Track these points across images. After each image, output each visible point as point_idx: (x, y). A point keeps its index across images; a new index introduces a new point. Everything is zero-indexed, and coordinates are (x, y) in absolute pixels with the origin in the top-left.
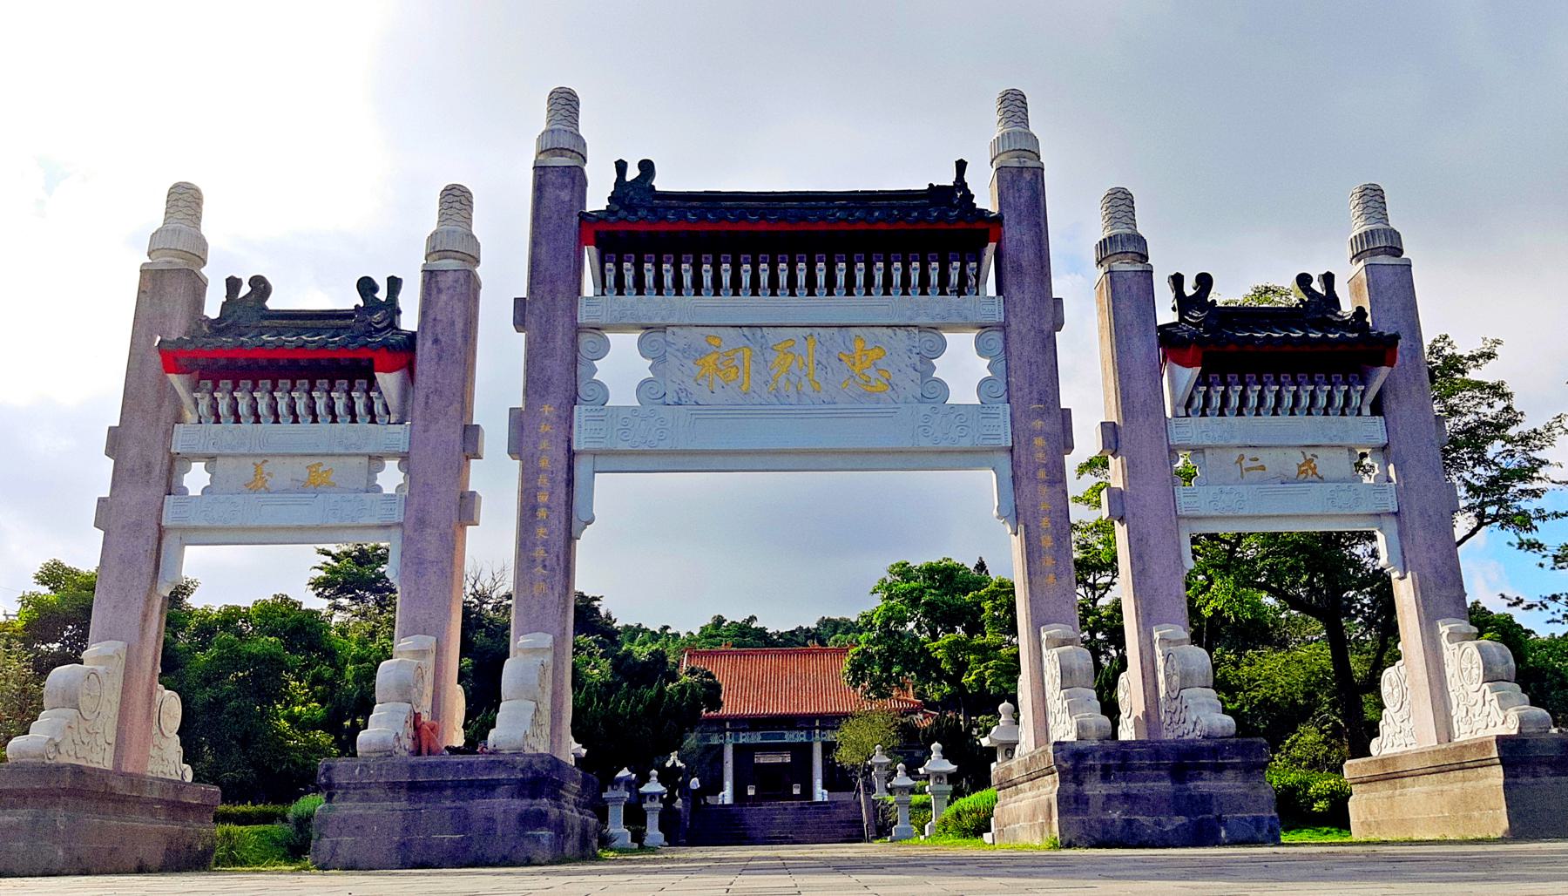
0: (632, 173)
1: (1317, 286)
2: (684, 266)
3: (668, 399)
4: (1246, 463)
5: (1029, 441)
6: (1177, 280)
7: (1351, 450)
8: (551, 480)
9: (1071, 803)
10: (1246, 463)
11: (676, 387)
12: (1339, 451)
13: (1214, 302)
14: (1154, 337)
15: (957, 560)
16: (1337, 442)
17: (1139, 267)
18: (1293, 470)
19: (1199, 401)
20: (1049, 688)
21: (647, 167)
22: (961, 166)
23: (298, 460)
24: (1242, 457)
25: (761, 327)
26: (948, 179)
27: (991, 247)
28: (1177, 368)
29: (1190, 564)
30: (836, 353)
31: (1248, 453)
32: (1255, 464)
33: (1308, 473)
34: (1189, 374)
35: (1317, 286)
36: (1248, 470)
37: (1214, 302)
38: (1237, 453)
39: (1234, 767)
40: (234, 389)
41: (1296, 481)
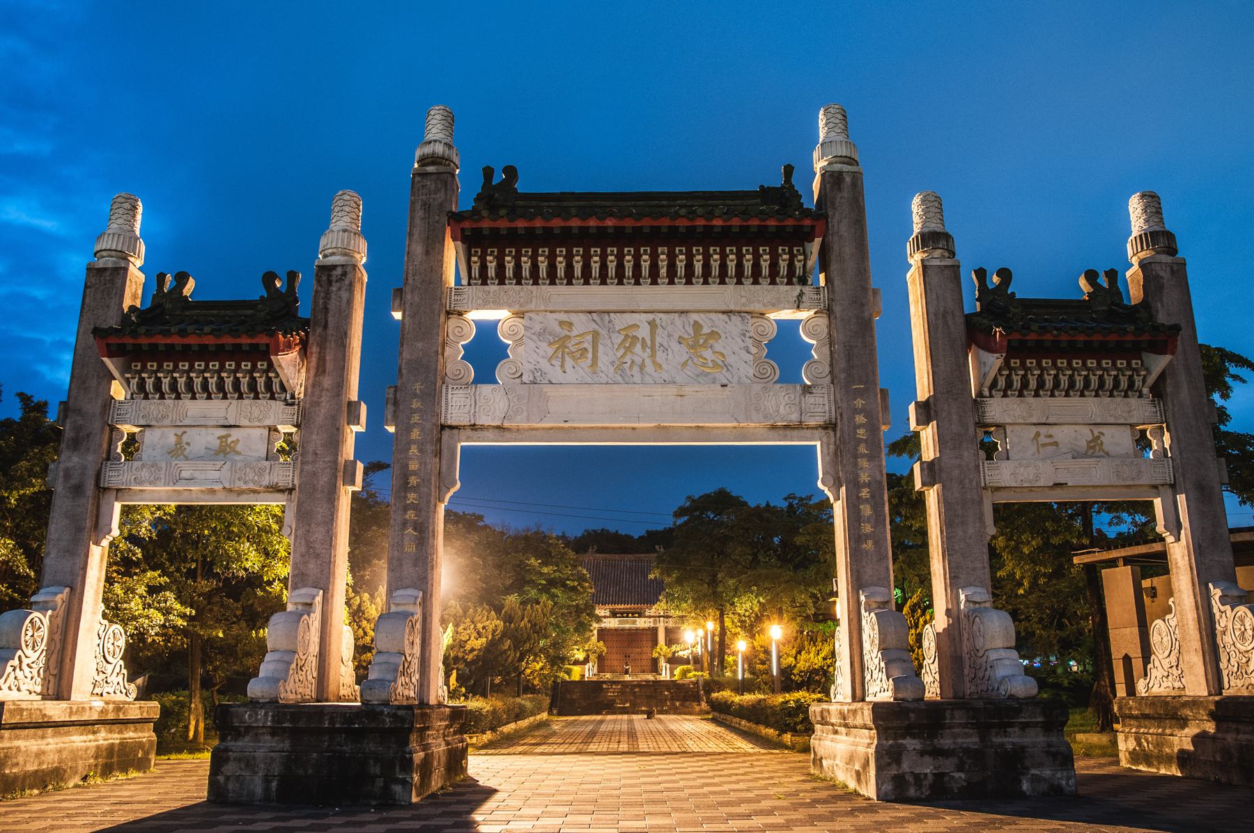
0: (499, 177)
1: (1103, 282)
2: (540, 259)
3: (525, 378)
4: (1042, 440)
5: (851, 419)
6: (981, 274)
7: (1132, 426)
8: (421, 451)
9: (887, 757)
10: (1042, 440)
11: (532, 367)
12: (1122, 428)
13: (1013, 294)
14: (960, 321)
15: (745, 499)
16: (1122, 421)
17: (948, 262)
18: (1083, 444)
19: (1002, 382)
20: (867, 646)
21: (511, 172)
22: (789, 170)
23: (211, 430)
24: (1038, 434)
25: (608, 312)
26: (779, 182)
27: (818, 241)
28: (982, 352)
29: (992, 531)
30: (676, 337)
31: (1043, 430)
32: (1048, 440)
33: (1094, 449)
34: (994, 361)
35: (1103, 282)
36: (1044, 445)
37: (1013, 294)
38: (1034, 429)
39: (1036, 724)
40: (142, 371)
41: (1085, 455)
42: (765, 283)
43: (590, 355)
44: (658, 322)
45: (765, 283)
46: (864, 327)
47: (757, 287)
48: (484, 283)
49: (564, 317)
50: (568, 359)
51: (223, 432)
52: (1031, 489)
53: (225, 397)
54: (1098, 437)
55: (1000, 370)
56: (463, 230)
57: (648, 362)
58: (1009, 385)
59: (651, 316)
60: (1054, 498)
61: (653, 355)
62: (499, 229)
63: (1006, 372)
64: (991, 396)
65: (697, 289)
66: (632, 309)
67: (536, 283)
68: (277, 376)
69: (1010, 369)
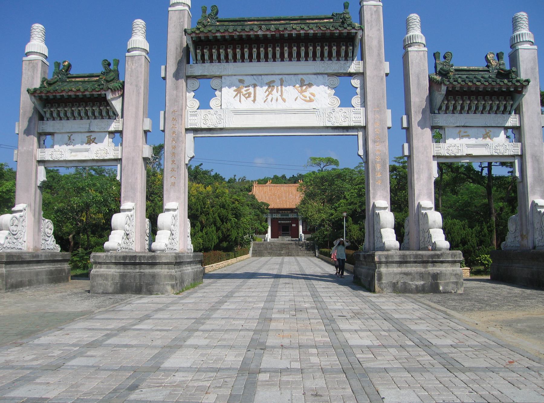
19: (444, 108)
24: (460, 132)
25: (261, 75)
32: (465, 134)
42: (326, 59)
43: (252, 95)
44: (284, 79)
45: (326, 59)
46: (364, 84)
47: (331, 62)
48: (204, 62)
49: (241, 78)
50: (242, 97)
51: (89, 134)
52: (456, 157)
53: (88, 119)
54: (488, 133)
55: (443, 101)
56: (192, 37)
57: (279, 98)
58: (447, 108)
59: (281, 77)
60: (400, 294)
61: (281, 95)
62: (242, 35)
63: (446, 102)
64: (439, 113)
65: (303, 63)
66: (272, 73)
67: (227, 62)
68: (111, 108)
69: (448, 101)
